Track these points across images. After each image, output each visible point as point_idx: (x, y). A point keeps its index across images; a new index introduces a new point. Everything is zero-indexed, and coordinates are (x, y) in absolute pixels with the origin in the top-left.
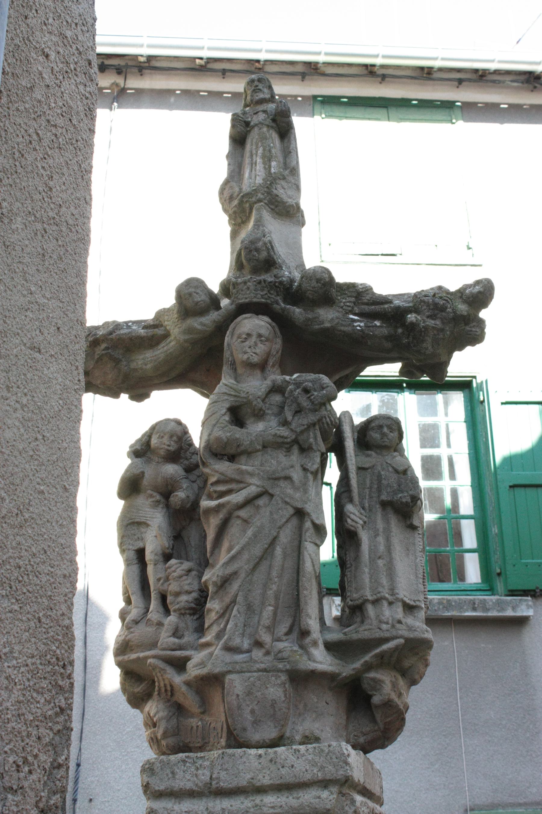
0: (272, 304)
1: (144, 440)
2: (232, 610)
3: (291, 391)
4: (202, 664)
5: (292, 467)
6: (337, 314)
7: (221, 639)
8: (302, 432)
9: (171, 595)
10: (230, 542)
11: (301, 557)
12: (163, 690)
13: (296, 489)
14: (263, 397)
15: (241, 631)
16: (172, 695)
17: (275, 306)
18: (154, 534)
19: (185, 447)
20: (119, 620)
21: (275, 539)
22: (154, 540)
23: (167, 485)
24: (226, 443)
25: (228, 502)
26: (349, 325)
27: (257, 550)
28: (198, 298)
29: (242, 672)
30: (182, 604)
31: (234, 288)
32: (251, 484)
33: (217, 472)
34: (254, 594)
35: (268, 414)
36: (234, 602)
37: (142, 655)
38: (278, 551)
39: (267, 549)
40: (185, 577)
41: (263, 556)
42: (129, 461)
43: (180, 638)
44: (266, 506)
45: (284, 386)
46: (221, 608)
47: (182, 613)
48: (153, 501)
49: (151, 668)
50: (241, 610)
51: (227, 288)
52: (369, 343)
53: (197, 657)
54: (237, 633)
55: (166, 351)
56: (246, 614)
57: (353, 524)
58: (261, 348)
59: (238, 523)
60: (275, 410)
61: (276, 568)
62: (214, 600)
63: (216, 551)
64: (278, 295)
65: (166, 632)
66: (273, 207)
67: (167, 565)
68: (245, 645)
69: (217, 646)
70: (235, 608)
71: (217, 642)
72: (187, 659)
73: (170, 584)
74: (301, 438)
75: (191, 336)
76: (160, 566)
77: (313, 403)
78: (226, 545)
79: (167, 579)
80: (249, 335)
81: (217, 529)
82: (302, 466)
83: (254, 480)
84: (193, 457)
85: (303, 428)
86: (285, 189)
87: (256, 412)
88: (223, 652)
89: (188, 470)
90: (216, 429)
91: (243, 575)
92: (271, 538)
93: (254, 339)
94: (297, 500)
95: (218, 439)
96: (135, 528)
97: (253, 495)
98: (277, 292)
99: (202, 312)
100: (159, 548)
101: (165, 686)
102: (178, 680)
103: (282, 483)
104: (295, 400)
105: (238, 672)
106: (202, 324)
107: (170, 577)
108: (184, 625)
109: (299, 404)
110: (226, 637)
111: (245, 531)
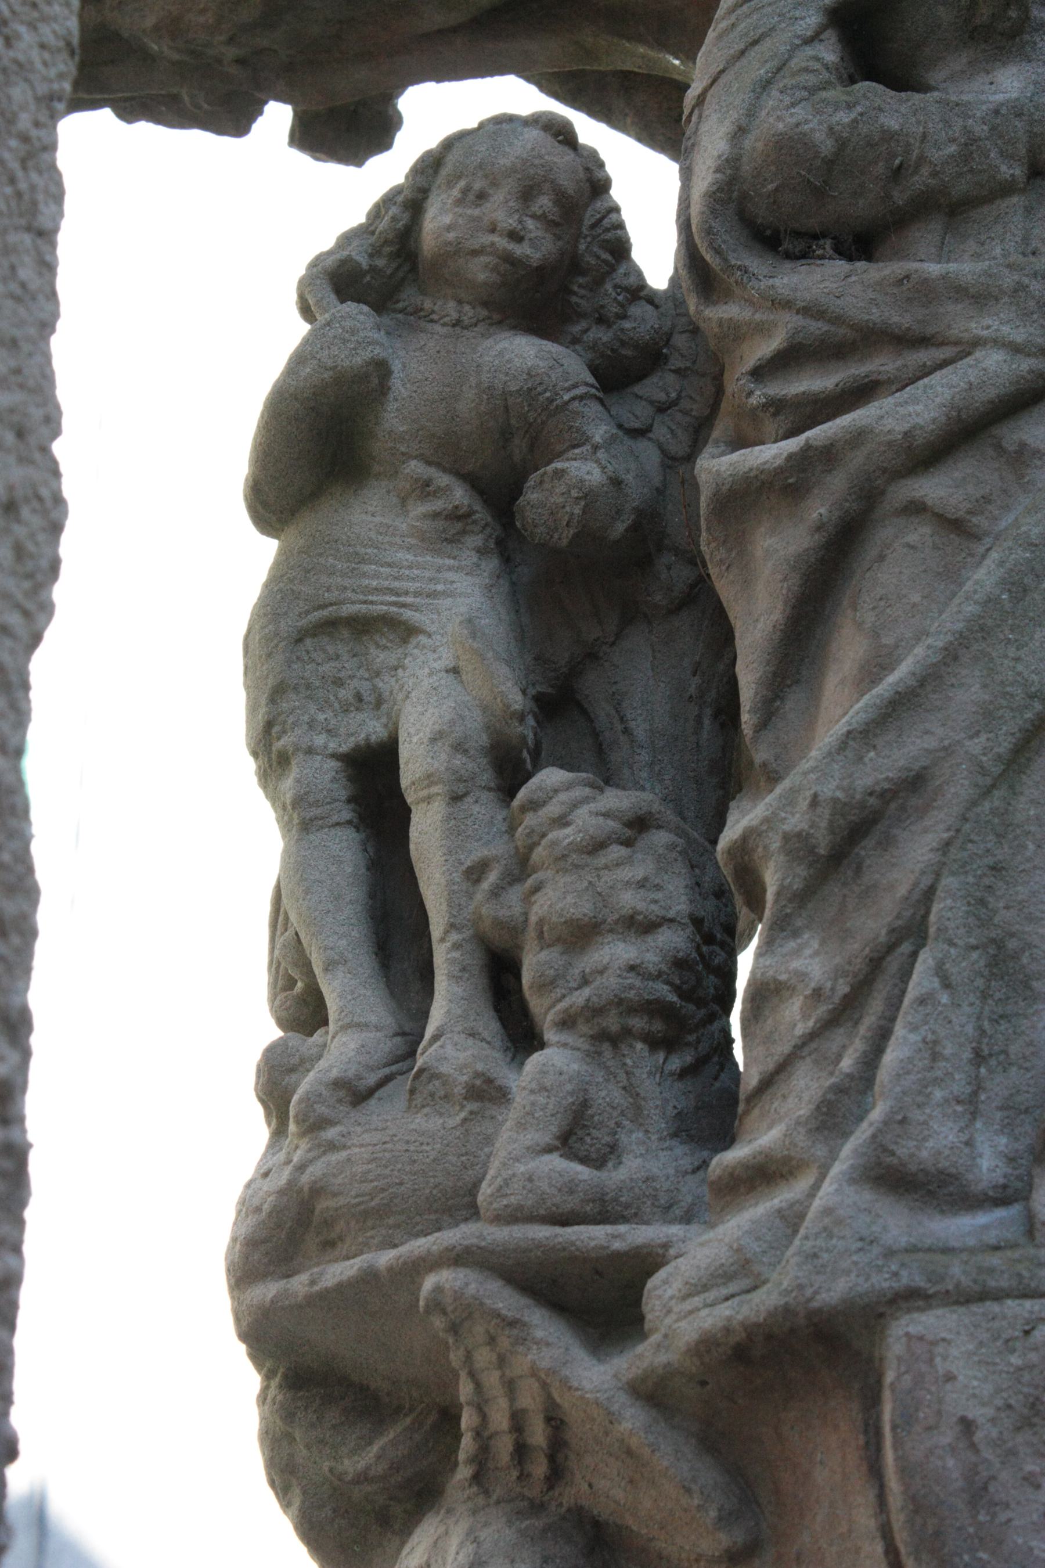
1: (383, 225)
2: (906, 974)
4: (740, 1272)
7: (846, 1135)
9: (544, 943)
10: (876, 635)
12: (504, 1447)
15: (959, 1085)
16: (556, 1474)
18: (446, 658)
20: (258, 1111)
22: (445, 680)
23: (506, 434)
24: (830, 163)
25: (858, 437)
29: (984, 1296)
30: (610, 983)
32: (977, 343)
33: (787, 304)
34: (1022, 892)
36: (913, 931)
37: (384, 1259)
40: (616, 852)
42: (265, 550)
43: (598, 1162)
46: (838, 973)
47: (605, 1031)
48: (436, 515)
49: (438, 1323)
50: (959, 971)
53: (697, 1250)
54: (938, 1094)
56: (985, 996)
59: (912, 538)
62: (796, 934)
65: (521, 1126)
67: (516, 803)
68: (985, 1163)
69: (824, 1171)
70: (925, 961)
71: (820, 1151)
72: (646, 1263)
73: (537, 889)
76: (482, 808)
78: (847, 649)
79: (521, 867)
83: (998, 323)
88: (866, 1196)
89: (614, 376)
90: (772, 100)
91: (957, 788)
95: (789, 147)
96: (342, 649)
97: (991, 393)
100: (474, 724)
101: (518, 1422)
102: (595, 1377)
105: (962, 1298)
107: (539, 854)
108: (618, 1096)
110: (876, 1115)
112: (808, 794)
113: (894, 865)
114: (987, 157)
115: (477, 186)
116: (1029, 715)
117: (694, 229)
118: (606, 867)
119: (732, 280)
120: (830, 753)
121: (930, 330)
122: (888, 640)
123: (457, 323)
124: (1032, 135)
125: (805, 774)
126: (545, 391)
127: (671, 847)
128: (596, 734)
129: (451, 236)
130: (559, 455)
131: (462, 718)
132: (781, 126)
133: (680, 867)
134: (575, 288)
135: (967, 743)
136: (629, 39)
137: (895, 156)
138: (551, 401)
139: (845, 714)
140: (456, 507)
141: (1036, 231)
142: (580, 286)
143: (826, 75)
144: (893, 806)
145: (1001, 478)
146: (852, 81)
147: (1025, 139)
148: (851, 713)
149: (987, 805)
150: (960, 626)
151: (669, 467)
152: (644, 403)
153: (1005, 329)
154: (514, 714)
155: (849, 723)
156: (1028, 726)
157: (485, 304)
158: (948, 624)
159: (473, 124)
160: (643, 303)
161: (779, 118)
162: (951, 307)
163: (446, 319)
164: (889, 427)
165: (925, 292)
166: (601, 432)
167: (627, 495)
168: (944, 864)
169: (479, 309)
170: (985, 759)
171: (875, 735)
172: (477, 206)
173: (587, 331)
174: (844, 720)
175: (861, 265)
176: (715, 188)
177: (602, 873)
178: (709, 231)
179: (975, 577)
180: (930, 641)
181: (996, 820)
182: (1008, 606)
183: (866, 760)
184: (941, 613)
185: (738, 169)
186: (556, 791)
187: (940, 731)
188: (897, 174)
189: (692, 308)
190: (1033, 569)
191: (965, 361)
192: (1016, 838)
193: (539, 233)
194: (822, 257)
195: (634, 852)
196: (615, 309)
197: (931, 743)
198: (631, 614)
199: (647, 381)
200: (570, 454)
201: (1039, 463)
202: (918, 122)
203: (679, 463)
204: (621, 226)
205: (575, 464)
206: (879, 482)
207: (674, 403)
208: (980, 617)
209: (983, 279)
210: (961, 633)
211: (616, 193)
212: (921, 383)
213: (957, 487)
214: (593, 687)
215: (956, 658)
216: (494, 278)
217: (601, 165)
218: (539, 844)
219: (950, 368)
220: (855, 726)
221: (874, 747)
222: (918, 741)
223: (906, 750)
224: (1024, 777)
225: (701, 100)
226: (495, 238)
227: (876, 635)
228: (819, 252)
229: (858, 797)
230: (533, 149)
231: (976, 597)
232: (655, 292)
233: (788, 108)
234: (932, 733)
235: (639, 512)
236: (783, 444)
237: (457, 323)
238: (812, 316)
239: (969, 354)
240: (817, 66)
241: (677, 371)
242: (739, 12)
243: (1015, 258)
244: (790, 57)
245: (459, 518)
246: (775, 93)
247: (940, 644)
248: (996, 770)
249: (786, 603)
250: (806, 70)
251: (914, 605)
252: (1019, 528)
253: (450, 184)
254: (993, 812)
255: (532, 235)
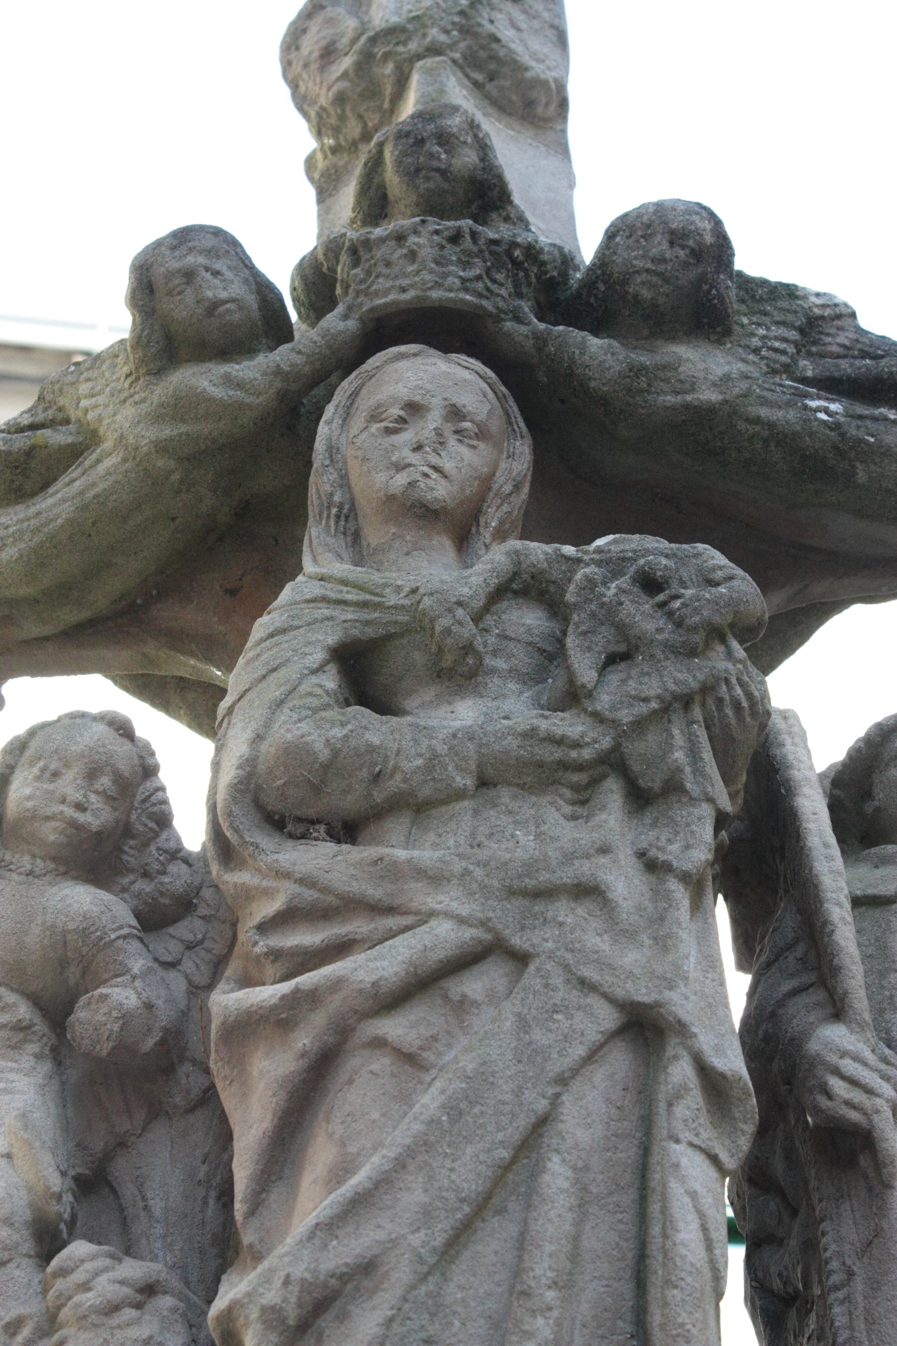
0: (498, 320)
3: (591, 583)
5: (604, 850)
6: (738, 367)
8: (640, 725)
10: (343, 1145)
11: (655, 1208)
13: (626, 936)
14: (478, 603)
17: (509, 325)
19: (140, 823)
21: (542, 1123)
23: (63, 963)
24: (326, 767)
25: (336, 984)
26: (789, 404)
27: (466, 1170)
28: (214, 290)
31: (356, 263)
32: (432, 914)
33: (287, 875)
35: (493, 671)
38: (556, 1175)
39: (507, 1167)
40: (129, 1313)
41: (488, 1196)
44: (493, 999)
45: (556, 575)
51: (319, 282)
52: (862, 477)
55: (82, 493)
57: (857, 1096)
58: (462, 459)
59: (375, 1067)
60: (522, 658)
61: (549, 1248)
63: (274, 1197)
64: (519, 295)
66: (479, 77)
67: (49, 1269)
74: (638, 750)
75: (184, 428)
77: (679, 624)
78: (320, 1155)
80: (414, 409)
81: (283, 1095)
82: (641, 855)
83: (447, 899)
84: (173, 868)
85: (643, 709)
86: (519, 29)
87: (448, 660)
89: (153, 920)
90: (285, 714)
91: (400, 1273)
92: (523, 1122)
93: (434, 419)
94: (630, 975)
95: (295, 753)
97: (441, 954)
98: (517, 285)
99: (231, 346)
103: (563, 911)
104: (609, 615)
106: (228, 381)
107: (65, 1314)
109: (622, 629)
111: (405, 1099)
112: (282, 1274)
113: (348, 1336)
114: (446, 770)
115: (53, 767)
116: (459, 1216)
117: (218, 810)
118: (119, 1327)
119: (246, 853)
120: (301, 1241)
121: (397, 902)
122: (352, 1149)
123: (30, 873)
124: (481, 755)
125: (281, 1257)
126: (96, 930)
127: (174, 1310)
128: (122, 1209)
129: (30, 804)
130: (105, 982)
131: (11, 1196)
132: (289, 736)
133: (180, 1327)
134: (126, 849)
135: (410, 1237)
136: (183, 653)
137: (376, 764)
138: (101, 938)
139: (316, 1208)
140: (20, 1020)
141: (481, 829)
142: (130, 847)
143: (326, 699)
144: (349, 1286)
145: (447, 1022)
146: (348, 704)
147: (475, 757)
148: (319, 1209)
149: (423, 1289)
150: (408, 1141)
151: (193, 994)
152: (175, 941)
153: (454, 905)
154: (53, 1195)
155: (317, 1216)
156: (458, 1225)
157: (54, 859)
158: (399, 1139)
159: (53, 717)
160: (180, 862)
161: (288, 730)
162: (413, 885)
163: (22, 870)
164: (361, 978)
165: (393, 872)
166: (139, 965)
167: (156, 1016)
168: (387, 1337)
169: (48, 863)
170: (422, 1251)
171: (338, 1228)
172: (52, 782)
173: (133, 883)
174: (314, 1214)
175: (345, 847)
176: (236, 781)
177: (115, 1332)
178: (230, 814)
179: (422, 1101)
180: (384, 1151)
181: (430, 1302)
182: (446, 1126)
183: (330, 1247)
184: (394, 1128)
185: (255, 767)
186: (83, 1261)
187: (389, 1226)
188: (377, 778)
189: (214, 873)
190: (467, 1097)
191: (422, 928)
192: (445, 1317)
193: (100, 806)
194: (316, 839)
195: (143, 1314)
196: (157, 866)
197: (381, 1235)
198: (156, 1111)
199: (180, 924)
200: (113, 982)
201: (476, 1011)
202: (395, 740)
203: (200, 990)
204: (165, 802)
205: (117, 990)
206: (351, 1021)
207: (200, 943)
208: (425, 1134)
209: (438, 865)
210: (409, 1146)
211: (164, 776)
212: (387, 943)
213: (411, 1027)
214: (122, 1170)
215: (404, 1167)
216: (64, 840)
217: (153, 754)
218: (65, 1305)
219: (410, 933)
220: (322, 1219)
221: (337, 1237)
222: (372, 1234)
223: (361, 1241)
224: (453, 1266)
225: (230, 711)
226: (64, 808)
227: (343, 1145)
228: (315, 835)
229: (322, 1278)
230: (98, 740)
231: (422, 1117)
232: (190, 854)
233: (295, 723)
234: (383, 1227)
235: (166, 1031)
236: (278, 986)
237: (30, 873)
238: (306, 886)
239: (426, 922)
240: (319, 691)
241: (203, 918)
242: (263, 645)
243: (464, 849)
244: (300, 683)
245: (22, 1029)
246: (286, 711)
247: (392, 1155)
248: (432, 1260)
249: (274, 1115)
250: (310, 694)
251: (374, 1122)
252: (457, 1063)
253: (32, 764)
254: (429, 1294)
255: (94, 807)
